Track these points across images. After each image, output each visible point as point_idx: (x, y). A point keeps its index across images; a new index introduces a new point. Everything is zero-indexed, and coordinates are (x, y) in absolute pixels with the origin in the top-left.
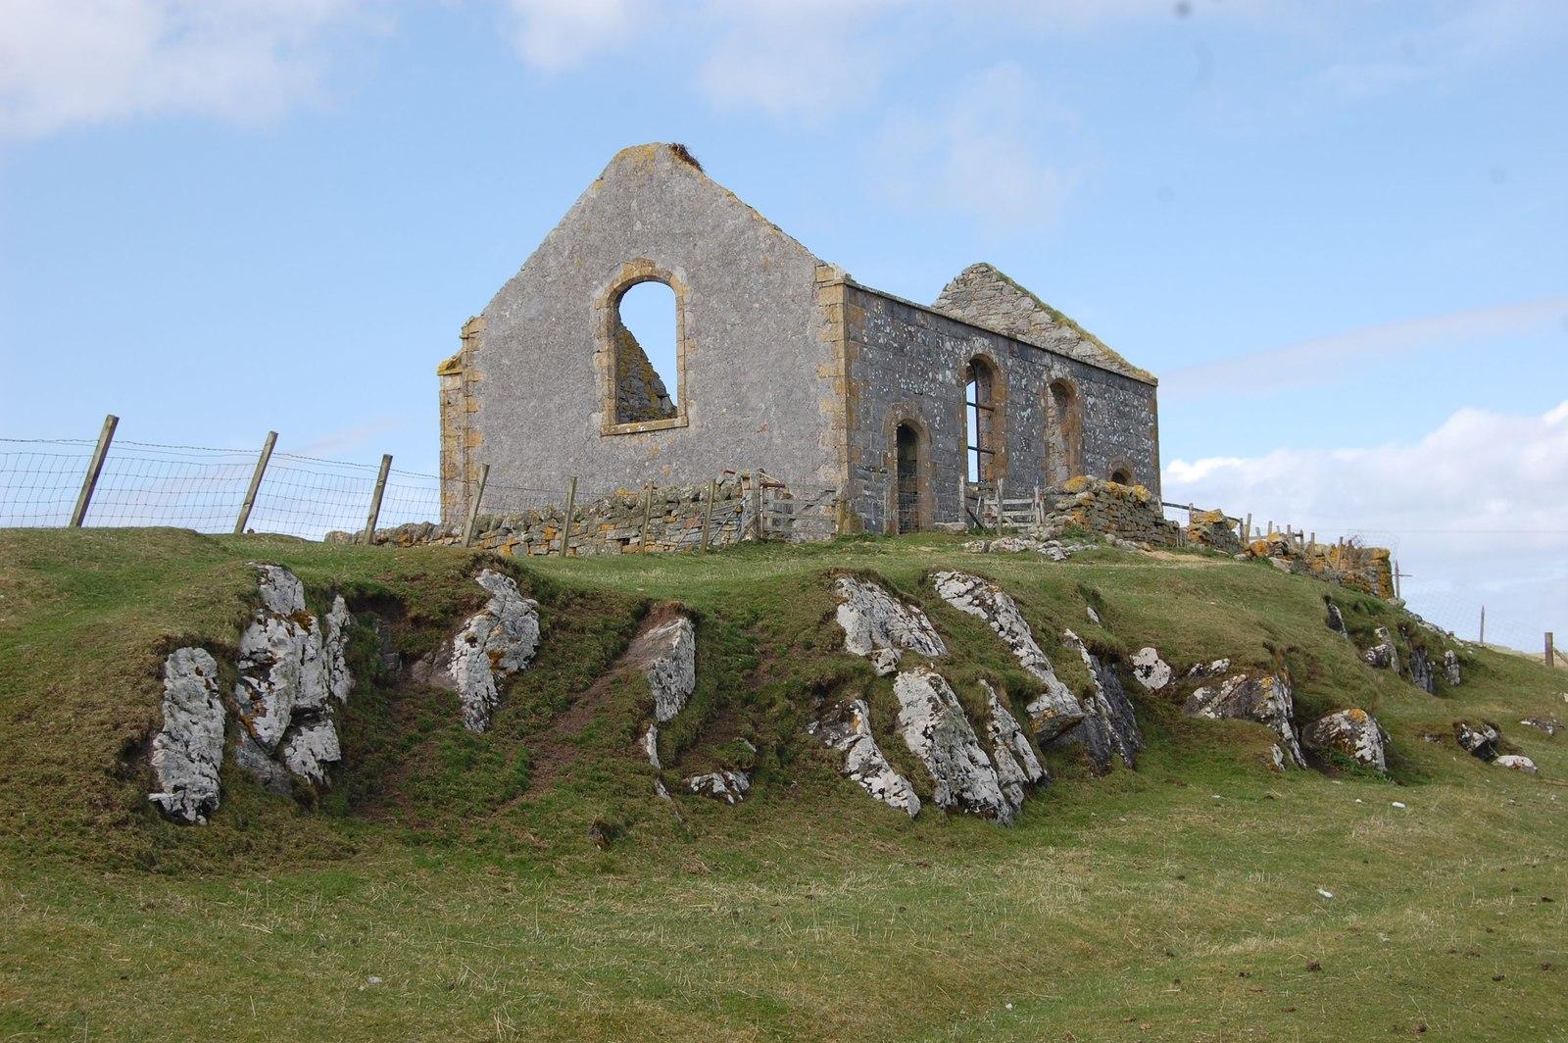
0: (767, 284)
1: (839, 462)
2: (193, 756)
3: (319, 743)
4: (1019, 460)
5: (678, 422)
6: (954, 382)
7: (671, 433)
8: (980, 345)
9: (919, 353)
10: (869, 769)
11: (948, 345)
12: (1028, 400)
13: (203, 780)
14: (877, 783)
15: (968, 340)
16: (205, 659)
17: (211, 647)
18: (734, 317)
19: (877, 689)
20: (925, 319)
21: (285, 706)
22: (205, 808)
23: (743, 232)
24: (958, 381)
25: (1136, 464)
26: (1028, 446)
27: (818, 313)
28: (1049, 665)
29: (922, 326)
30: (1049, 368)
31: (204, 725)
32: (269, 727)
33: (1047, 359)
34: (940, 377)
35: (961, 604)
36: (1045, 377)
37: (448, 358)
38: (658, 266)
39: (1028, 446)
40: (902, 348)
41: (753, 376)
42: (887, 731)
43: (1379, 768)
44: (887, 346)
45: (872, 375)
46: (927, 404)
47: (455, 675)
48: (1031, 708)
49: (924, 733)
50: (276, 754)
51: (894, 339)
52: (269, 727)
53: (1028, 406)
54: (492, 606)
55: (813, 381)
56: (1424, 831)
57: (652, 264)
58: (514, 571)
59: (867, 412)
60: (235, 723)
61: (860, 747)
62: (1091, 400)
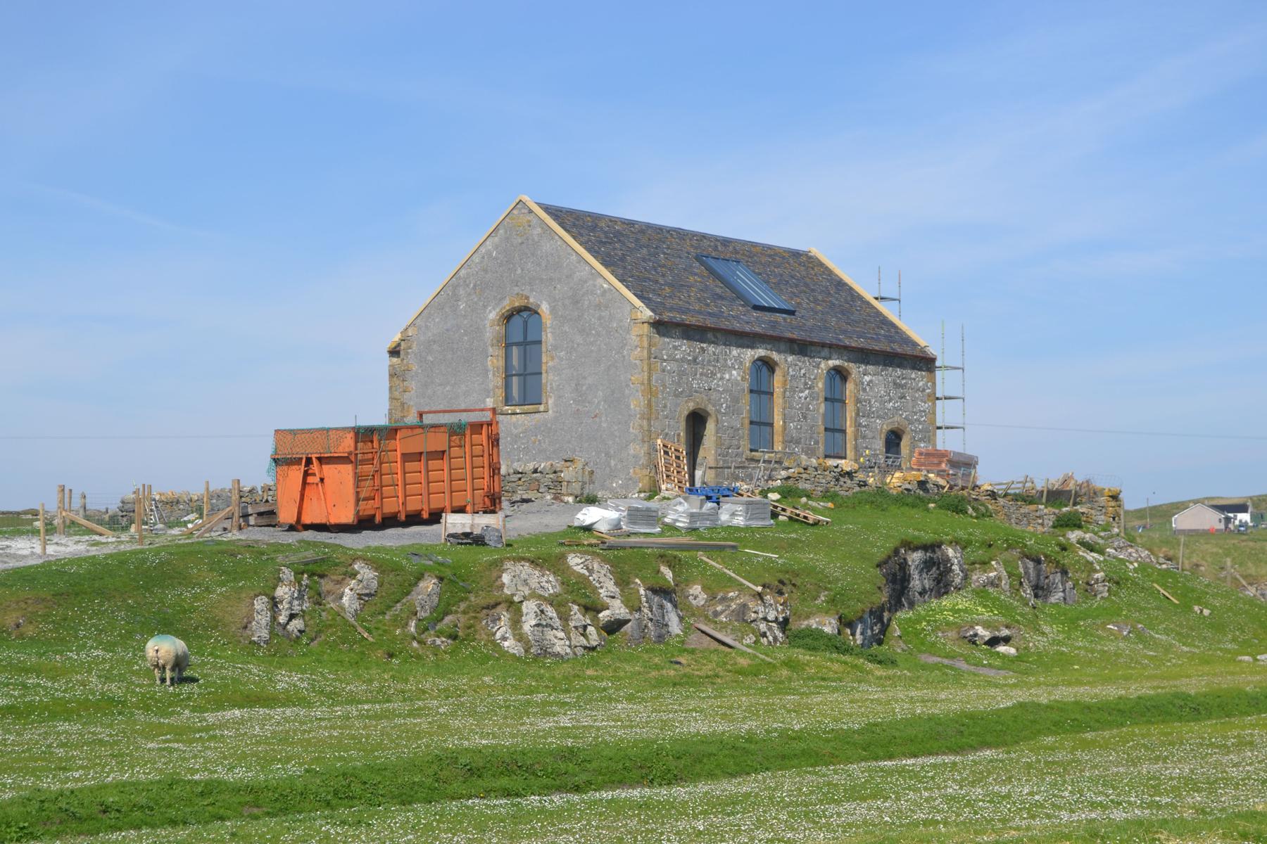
0: (600, 318)
1: (644, 442)
4: (796, 428)
5: (542, 408)
7: (537, 415)
9: (709, 361)
10: (504, 639)
12: (806, 384)
13: (265, 634)
14: (506, 644)
16: (265, 599)
17: (266, 595)
18: (579, 339)
19: (514, 606)
21: (288, 613)
22: (266, 642)
23: (586, 282)
25: (911, 423)
26: (805, 418)
27: (633, 338)
28: (618, 595)
31: (262, 619)
32: (282, 619)
34: (727, 376)
35: (578, 569)
37: (389, 345)
38: (531, 300)
40: (695, 360)
41: (590, 380)
42: (516, 623)
44: (683, 360)
45: (668, 381)
46: (714, 396)
47: (942, 482)
48: (601, 615)
50: (284, 626)
52: (282, 619)
54: (359, 577)
55: (627, 386)
57: (527, 298)
58: (366, 560)
59: (665, 407)
60: (274, 618)
61: (502, 629)
62: (867, 378)
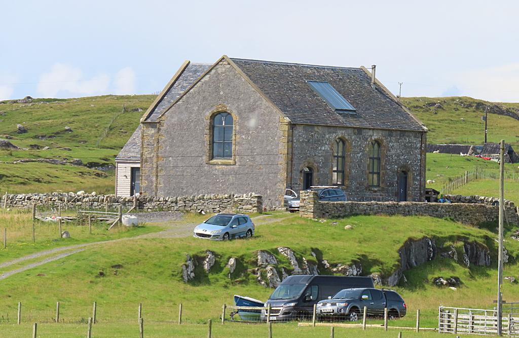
2: (138, 292)
3: (507, 261)
6: (329, 149)
8: (340, 133)
11: (327, 136)
12: (361, 149)
15: (336, 133)
20: (318, 129)
24: (330, 148)
29: (317, 131)
30: (371, 136)
33: (371, 132)
36: (369, 139)
39: (360, 167)
43: (18, 289)
49: (275, 288)
51: (306, 139)
53: (360, 152)
56: (138, 268)
62: (391, 144)
